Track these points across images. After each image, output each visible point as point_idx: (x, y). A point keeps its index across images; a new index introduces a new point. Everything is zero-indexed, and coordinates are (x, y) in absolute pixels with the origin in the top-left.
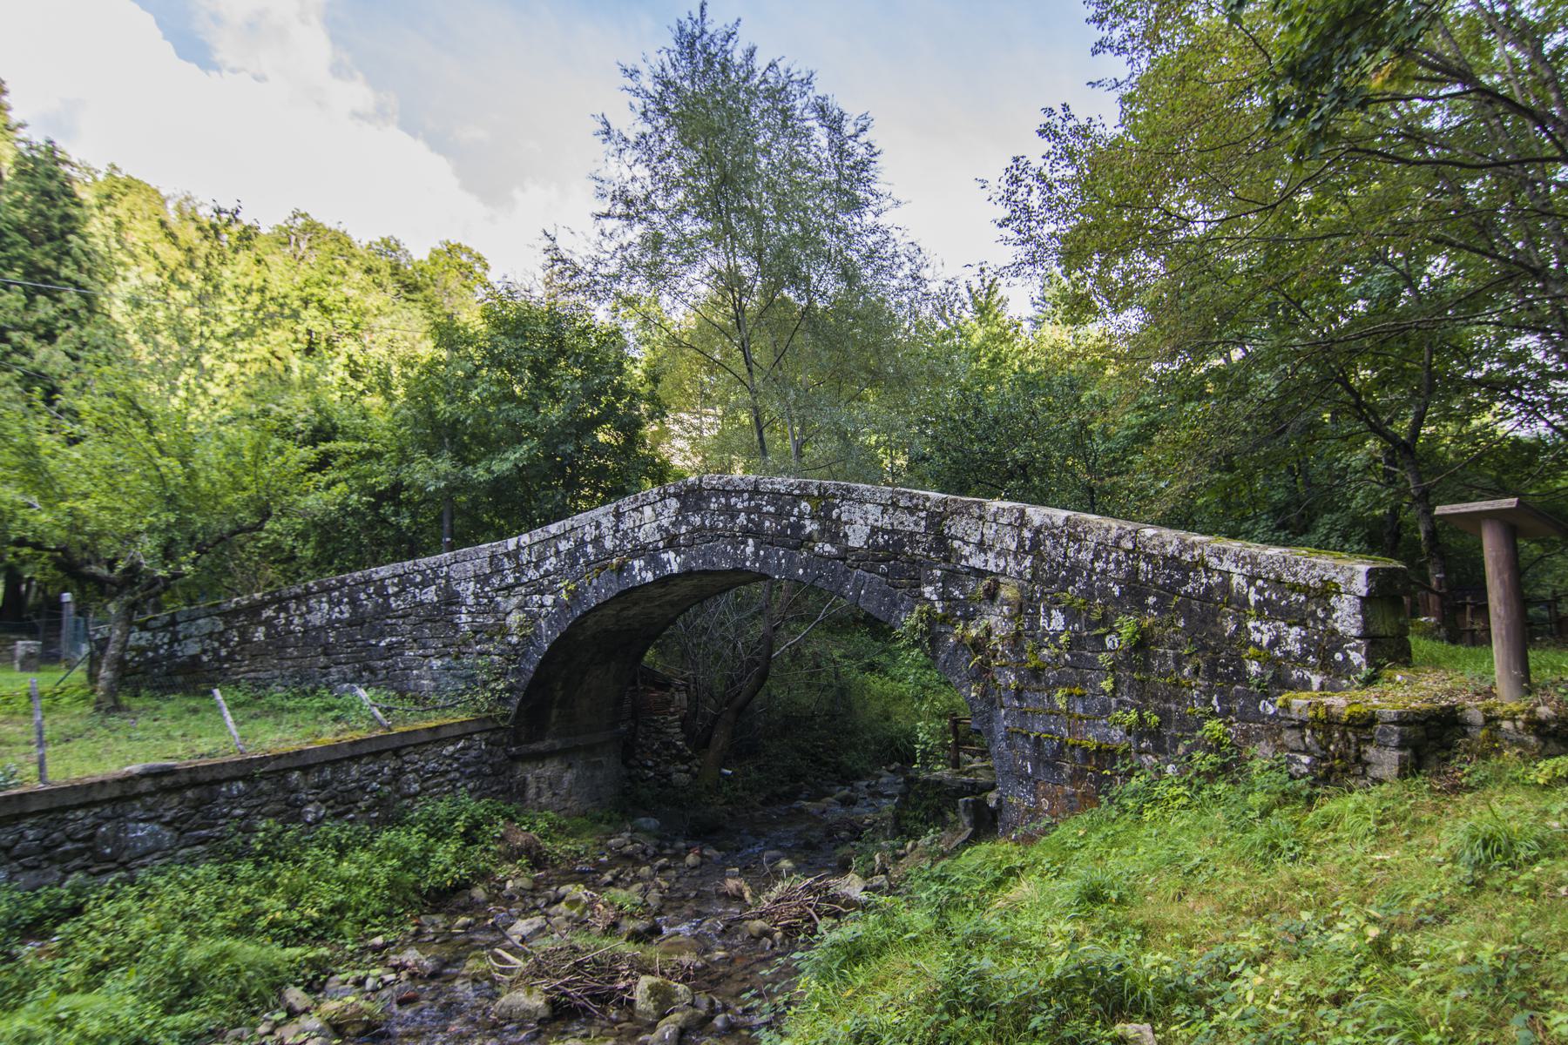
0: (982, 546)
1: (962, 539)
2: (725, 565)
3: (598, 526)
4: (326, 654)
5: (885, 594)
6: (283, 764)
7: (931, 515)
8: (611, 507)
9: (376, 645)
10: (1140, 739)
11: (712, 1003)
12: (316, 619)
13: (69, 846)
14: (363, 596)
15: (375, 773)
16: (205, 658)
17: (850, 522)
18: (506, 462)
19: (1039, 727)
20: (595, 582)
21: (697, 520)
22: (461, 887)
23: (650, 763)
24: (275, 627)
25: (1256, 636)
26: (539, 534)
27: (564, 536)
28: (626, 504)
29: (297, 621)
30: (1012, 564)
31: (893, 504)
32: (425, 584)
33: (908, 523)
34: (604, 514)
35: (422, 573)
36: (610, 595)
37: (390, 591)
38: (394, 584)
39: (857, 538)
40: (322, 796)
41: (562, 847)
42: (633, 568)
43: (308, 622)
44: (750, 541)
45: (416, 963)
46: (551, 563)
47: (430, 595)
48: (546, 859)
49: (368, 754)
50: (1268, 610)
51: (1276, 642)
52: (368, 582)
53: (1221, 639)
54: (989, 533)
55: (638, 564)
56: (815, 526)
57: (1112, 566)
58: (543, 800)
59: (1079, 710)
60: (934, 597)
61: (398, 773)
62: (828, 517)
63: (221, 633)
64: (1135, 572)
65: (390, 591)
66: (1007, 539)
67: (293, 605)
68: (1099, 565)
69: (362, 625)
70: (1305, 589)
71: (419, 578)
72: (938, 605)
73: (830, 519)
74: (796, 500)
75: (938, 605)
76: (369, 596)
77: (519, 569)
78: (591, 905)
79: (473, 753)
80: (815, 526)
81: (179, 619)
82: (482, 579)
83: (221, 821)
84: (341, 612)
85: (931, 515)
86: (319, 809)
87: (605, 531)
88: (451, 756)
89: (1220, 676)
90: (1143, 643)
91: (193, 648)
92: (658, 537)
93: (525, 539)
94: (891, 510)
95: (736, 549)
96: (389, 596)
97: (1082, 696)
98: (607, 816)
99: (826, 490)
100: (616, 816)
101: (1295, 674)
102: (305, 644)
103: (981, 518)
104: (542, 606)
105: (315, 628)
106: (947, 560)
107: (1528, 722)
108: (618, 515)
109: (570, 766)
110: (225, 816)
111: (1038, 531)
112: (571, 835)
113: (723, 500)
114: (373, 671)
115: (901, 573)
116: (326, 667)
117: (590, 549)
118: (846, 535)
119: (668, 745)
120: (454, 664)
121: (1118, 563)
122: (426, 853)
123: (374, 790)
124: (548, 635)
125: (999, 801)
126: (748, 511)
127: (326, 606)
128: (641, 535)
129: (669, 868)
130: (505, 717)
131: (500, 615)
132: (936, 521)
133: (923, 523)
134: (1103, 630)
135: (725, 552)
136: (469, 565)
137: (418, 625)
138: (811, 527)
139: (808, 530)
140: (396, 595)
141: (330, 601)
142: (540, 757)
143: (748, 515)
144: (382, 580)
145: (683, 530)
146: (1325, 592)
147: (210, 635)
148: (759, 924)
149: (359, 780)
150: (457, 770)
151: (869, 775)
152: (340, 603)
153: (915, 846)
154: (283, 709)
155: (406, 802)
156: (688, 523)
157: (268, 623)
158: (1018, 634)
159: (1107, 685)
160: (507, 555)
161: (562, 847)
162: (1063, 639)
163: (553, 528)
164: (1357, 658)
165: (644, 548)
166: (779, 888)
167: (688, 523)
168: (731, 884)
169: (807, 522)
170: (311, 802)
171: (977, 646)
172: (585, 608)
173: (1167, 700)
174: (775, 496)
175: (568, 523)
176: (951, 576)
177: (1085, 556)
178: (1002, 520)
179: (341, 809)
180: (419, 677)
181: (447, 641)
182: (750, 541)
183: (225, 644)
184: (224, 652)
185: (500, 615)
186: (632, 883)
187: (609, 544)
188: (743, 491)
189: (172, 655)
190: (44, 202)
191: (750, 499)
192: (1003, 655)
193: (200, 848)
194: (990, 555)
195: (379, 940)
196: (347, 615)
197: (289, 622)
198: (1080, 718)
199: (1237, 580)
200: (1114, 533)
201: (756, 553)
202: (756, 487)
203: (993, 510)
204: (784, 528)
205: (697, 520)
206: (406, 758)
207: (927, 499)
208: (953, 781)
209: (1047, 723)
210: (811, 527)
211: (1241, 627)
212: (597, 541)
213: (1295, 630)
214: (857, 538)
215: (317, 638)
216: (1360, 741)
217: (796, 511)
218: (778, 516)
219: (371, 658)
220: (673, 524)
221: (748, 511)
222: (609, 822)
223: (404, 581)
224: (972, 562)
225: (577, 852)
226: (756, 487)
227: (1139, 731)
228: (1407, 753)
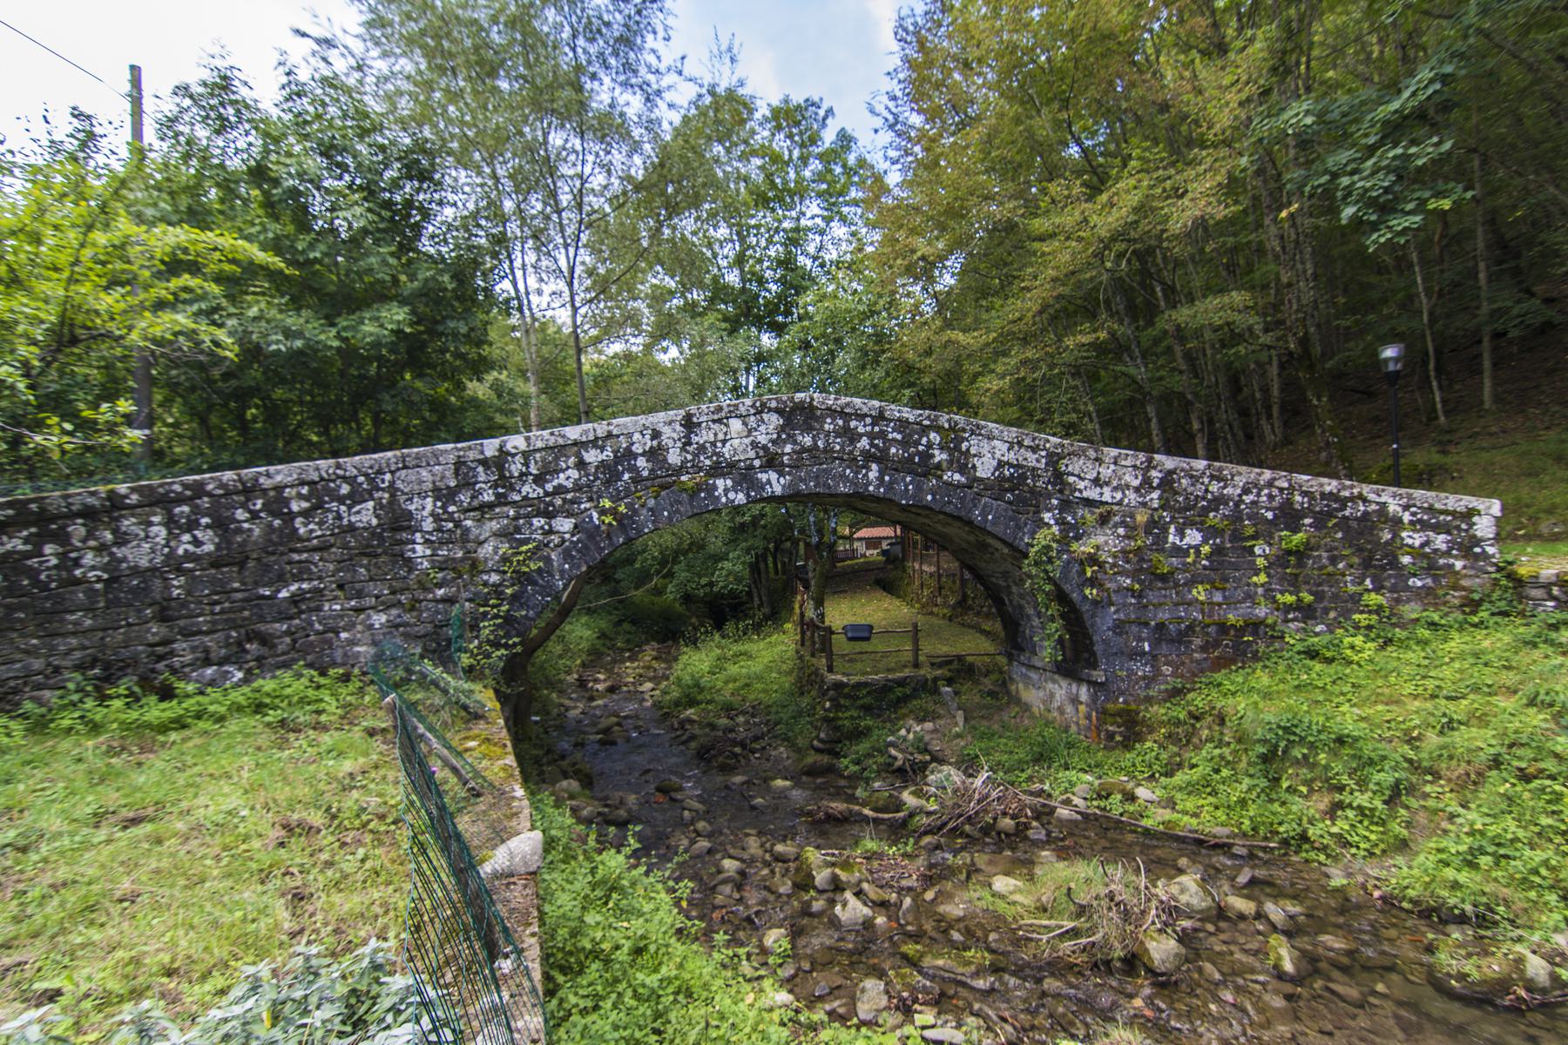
0: (1097, 482)
1: (1079, 476)
4: (163, 617)
5: (1011, 519)
7: (1050, 455)
12: (139, 555)
14: (241, 514)
17: (979, 455)
19: (1164, 615)
21: (807, 440)
24: (33, 574)
25: (1410, 541)
27: (595, 443)
32: (356, 498)
35: (350, 480)
37: (295, 507)
38: (300, 497)
42: (715, 488)
43: (116, 561)
46: (568, 477)
47: (366, 515)
50: (1424, 526)
51: (1426, 543)
52: (249, 490)
53: (1378, 543)
56: (944, 456)
62: (957, 448)
64: (1289, 503)
65: (295, 507)
67: (78, 529)
68: (1248, 499)
69: (242, 565)
70: (1453, 513)
73: (960, 451)
74: (925, 430)
76: (254, 515)
77: (504, 481)
80: (944, 456)
82: (444, 495)
84: (197, 542)
87: (665, 440)
92: (752, 454)
95: (857, 473)
96: (291, 516)
105: (135, 571)
106: (1061, 491)
108: (689, 424)
114: (265, 640)
115: (1025, 502)
117: (641, 462)
118: (974, 467)
120: (407, 617)
121: (1271, 497)
126: (871, 436)
127: (159, 532)
128: (727, 451)
131: (470, 545)
132: (1053, 459)
135: (843, 476)
136: (424, 473)
137: (347, 563)
138: (939, 456)
139: (937, 459)
140: (305, 514)
141: (170, 522)
144: (279, 488)
145: (788, 448)
146: (1470, 513)
152: (192, 525)
156: (795, 442)
160: (484, 463)
163: (573, 433)
165: (732, 465)
167: (795, 442)
169: (936, 452)
173: (1320, 585)
174: (902, 424)
175: (601, 429)
182: (874, 467)
187: (674, 458)
188: (866, 415)
191: (873, 424)
196: (208, 548)
197: (68, 562)
201: (880, 479)
204: (911, 457)
205: (807, 440)
210: (939, 456)
211: (1395, 535)
212: (655, 454)
215: (141, 592)
217: (924, 440)
218: (904, 444)
219: (262, 619)
220: (774, 442)
221: (871, 436)
223: (319, 493)
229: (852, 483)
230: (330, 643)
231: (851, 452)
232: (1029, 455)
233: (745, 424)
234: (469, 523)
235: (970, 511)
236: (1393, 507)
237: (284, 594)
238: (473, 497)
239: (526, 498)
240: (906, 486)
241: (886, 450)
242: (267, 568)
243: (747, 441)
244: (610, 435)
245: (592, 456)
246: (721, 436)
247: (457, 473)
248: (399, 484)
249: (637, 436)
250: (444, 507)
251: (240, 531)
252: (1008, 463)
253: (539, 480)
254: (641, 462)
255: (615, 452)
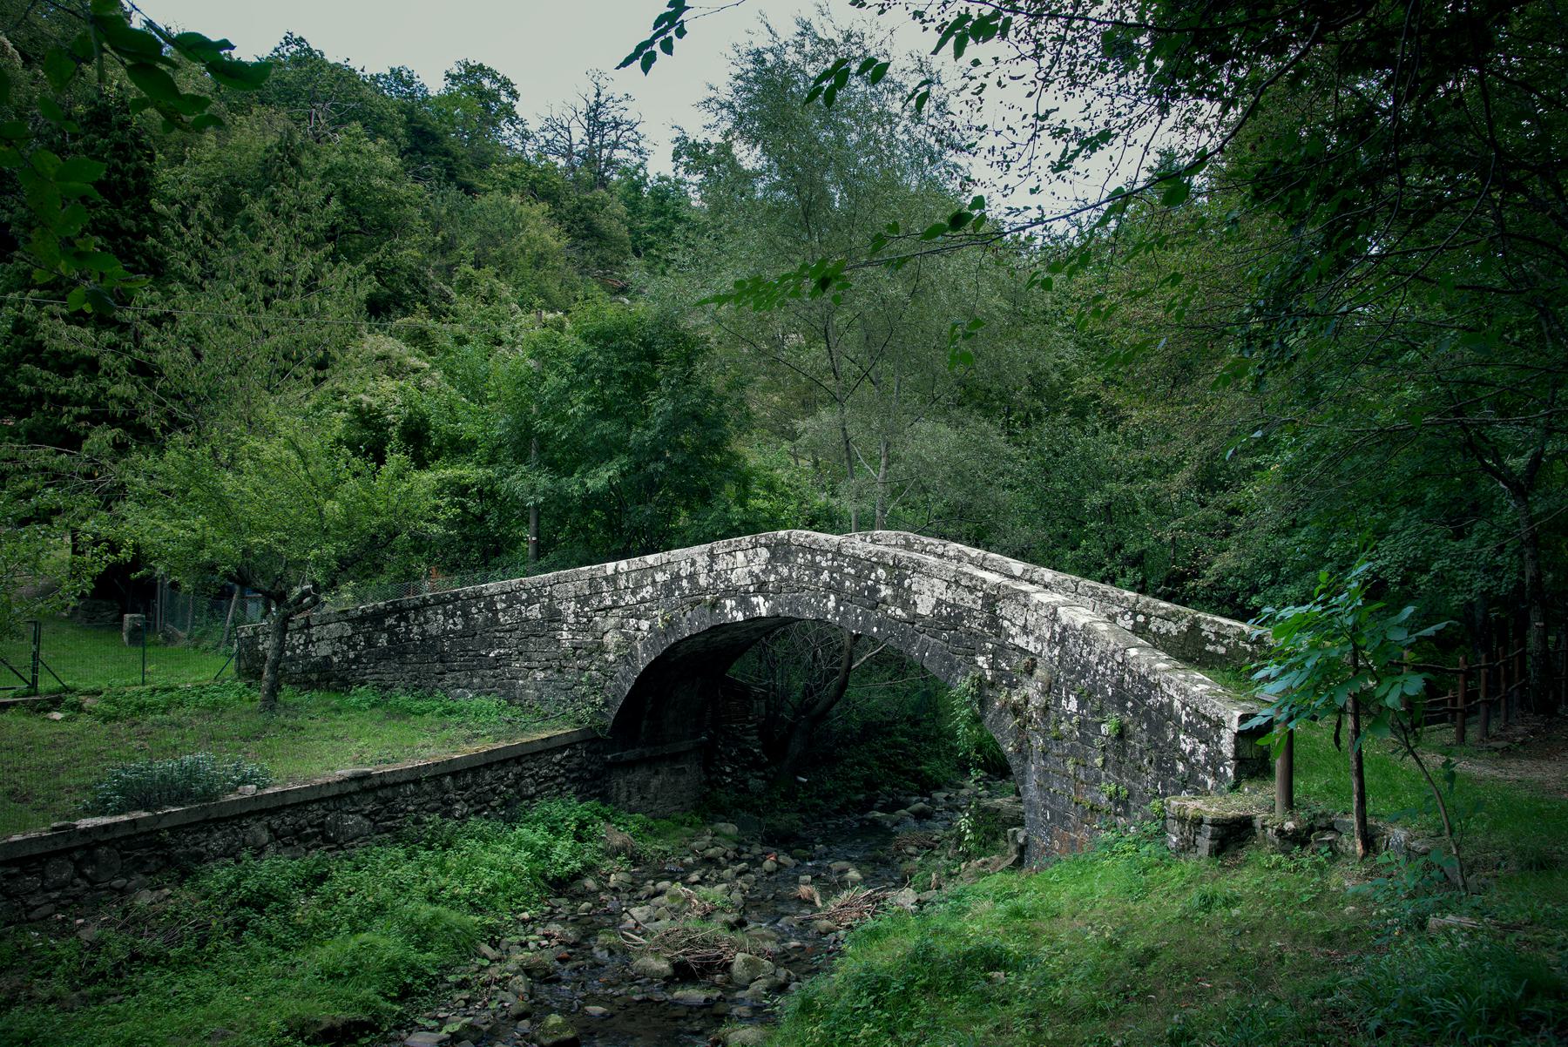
0: (1025, 630)
1: (1010, 620)
2: (809, 615)
3: (693, 563)
5: (946, 658)
6: (440, 770)
7: (986, 596)
8: (705, 547)
9: (487, 656)
10: (1117, 805)
11: (788, 975)
12: (433, 629)
13: (309, 830)
14: (474, 610)
15: (502, 778)
16: (335, 659)
17: (920, 593)
18: (601, 478)
20: (689, 614)
21: (785, 571)
22: (576, 876)
23: (728, 770)
24: (397, 635)
25: (1183, 746)
26: (636, 562)
27: (660, 568)
28: (720, 546)
29: (415, 629)
30: (1046, 649)
31: (956, 582)
32: (529, 602)
33: (968, 600)
34: (698, 552)
35: (527, 591)
36: (704, 628)
38: (502, 601)
39: (924, 607)
40: (467, 795)
41: (652, 847)
44: (832, 597)
45: (562, 933)
46: (647, 592)
47: (535, 612)
48: (639, 857)
49: (498, 762)
50: (1191, 730)
52: (478, 596)
54: (1032, 620)
55: (730, 603)
56: (889, 592)
57: (1109, 672)
58: (633, 803)
59: (1082, 777)
60: (985, 666)
61: (520, 777)
62: (900, 584)
63: (350, 638)
66: (1044, 628)
67: (412, 615)
71: (524, 596)
72: (989, 673)
75: (989, 673)
76: (480, 611)
78: (688, 900)
79: (576, 760)
80: (889, 592)
81: (312, 623)
82: (582, 600)
83: (400, 815)
84: (455, 624)
85: (986, 596)
86: (463, 807)
87: (699, 568)
88: (559, 763)
89: (1163, 769)
90: (1122, 734)
91: (324, 650)
92: (748, 581)
93: (623, 565)
94: (954, 587)
95: (819, 602)
97: (1085, 766)
98: (689, 820)
99: (900, 562)
100: (698, 819)
101: (1201, 776)
102: (423, 651)
103: (1025, 605)
104: (638, 629)
106: (998, 635)
107: (1278, 831)
108: (713, 557)
109: (657, 773)
110: (402, 811)
111: (1065, 629)
112: (658, 835)
113: (809, 557)
116: (442, 673)
117: (685, 583)
118: (915, 603)
119: (745, 752)
120: (556, 676)
121: (1113, 671)
122: (549, 847)
123: (501, 792)
124: (643, 660)
125: (1026, 838)
127: (441, 617)
128: (733, 577)
129: (748, 871)
130: (603, 728)
133: (980, 602)
134: (1098, 719)
135: (809, 603)
136: (570, 586)
139: (883, 594)
140: (504, 610)
141: (445, 614)
142: (630, 765)
143: (831, 573)
144: (492, 596)
145: (772, 578)
147: (340, 639)
148: (826, 923)
149: (490, 784)
150: (563, 775)
151: (951, 785)
153: (967, 867)
154: (409, 710)
155: (525, 802)
156: (777, 573)
157: (390, 630)
158: (1047, 708)
159: (1099, 761)
160: (606, 579)
161: (652, 847)
162: (1075, 720)
163: (651, 559)
164: (1230, 772)
166: (845, 896)
167: (777, 573)
168: (804, 890)
169: (883, 587)
170: (458, 801)
171: (1016, 711)
172: (679, 637)
174: (855, 561)
176: (1000, 651)
177: (1094, 659)
178: (1040, 612)
179: (479, 807)
180: (524, 687)
181: (549, 656)
182: (832, 597)
183: (353, 647)
184: (352, 655)
185: (599, 634)
186: (717, 883)
189: (307, 655)
190: (119, 157)
191: (833, 560)
192: (1036, 722)
193: (387, 835)
194: (1031, 638)
195: (525, 915)
196: (460, 627)
197: (409, 631)
198: (1082, 783)
199: (1176, 704)
200: (1111, 647)
201: (837, 608)
202: (839, 549)
203: (1035, 601)
204: (862, 590)
205: (785, 571)
206: (525, 765)
207: (984, 581)
208: (1010, 810)
209: (1061, 783)
210: (885, 591)
211: (1176, 737)
212: (692, 577)
213: (1203, 746)
214: (924, 607)
215: (433, 647)
216: (1196, 833)
217: (873, 575)
218: (858, 577)
220: (763, 571)
222: (691, 825)
223: (512, 597)
224: (1017, 641)
225: (665, 852)
226: (839, 549)
227: (1114, 798)
228: (1216, 842)
229: (814, 609)
230: (514, 685)
231: (816, 584)
232: (966, 595)
233: (746, 556)
234: (597, 619)
235: (909, 646)
236: (466, 747)
237: (492, 655)
238: (600, 602)
239: (627, 604)
240: (857, 617)
241: (841, 583)
242: (484, 639)
243: (746, 570)
244: (669, 562)
245: (660, 577)
246: (730, 566)
247: (590, 586)
248: (555, 593)
249: (683, 563)
250: (582, 608)
251: (473, 619)
252: (944, 602)
253: (634, 593)
254: (685, 583)
255: (671, 575)
